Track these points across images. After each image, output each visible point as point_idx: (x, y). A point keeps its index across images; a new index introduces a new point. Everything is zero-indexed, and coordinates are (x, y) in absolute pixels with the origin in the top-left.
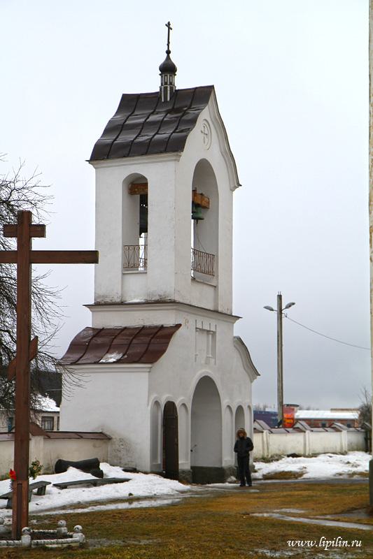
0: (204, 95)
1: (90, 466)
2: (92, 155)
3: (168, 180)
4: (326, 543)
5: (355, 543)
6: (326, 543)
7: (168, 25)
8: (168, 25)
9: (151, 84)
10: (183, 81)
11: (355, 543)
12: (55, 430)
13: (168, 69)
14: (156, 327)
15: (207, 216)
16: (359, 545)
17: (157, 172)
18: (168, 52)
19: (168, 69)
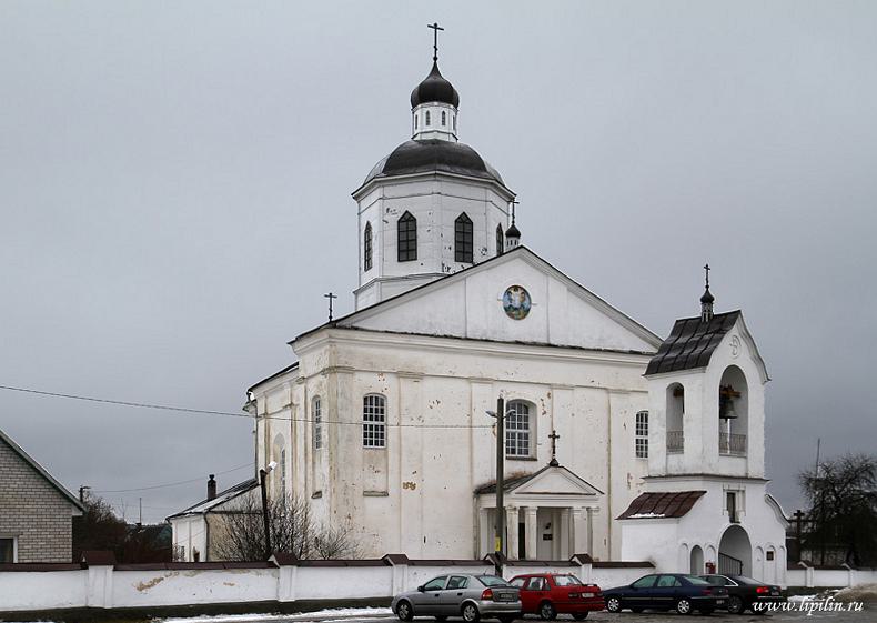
0: (730, 319)
1: (545, 413)
2: (230, 603)
3: (701, 388)
4: (809, 606)
5: (853, 607)
6: (809, 606)
7: (707, 267)
8: (707, 267)
9: (695, 311)
10: (717, 310)
11: (853, 607)
12: (555, 559)
13: (707, 300)
14: (660, 494)
15: (738, 404)
16: (860, 608)
17: (690, 381)
18: (707, 287)
19: (707, 300)
